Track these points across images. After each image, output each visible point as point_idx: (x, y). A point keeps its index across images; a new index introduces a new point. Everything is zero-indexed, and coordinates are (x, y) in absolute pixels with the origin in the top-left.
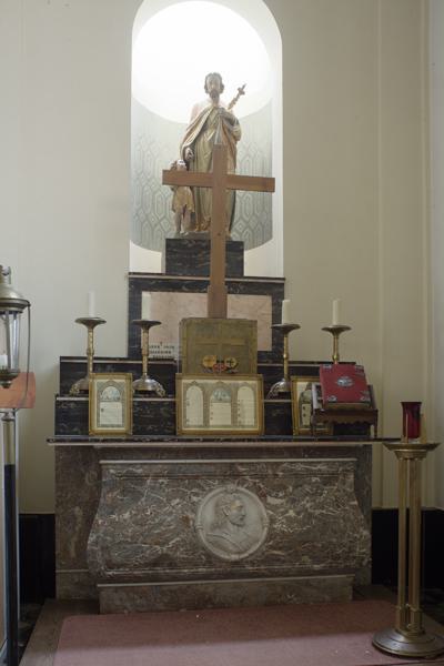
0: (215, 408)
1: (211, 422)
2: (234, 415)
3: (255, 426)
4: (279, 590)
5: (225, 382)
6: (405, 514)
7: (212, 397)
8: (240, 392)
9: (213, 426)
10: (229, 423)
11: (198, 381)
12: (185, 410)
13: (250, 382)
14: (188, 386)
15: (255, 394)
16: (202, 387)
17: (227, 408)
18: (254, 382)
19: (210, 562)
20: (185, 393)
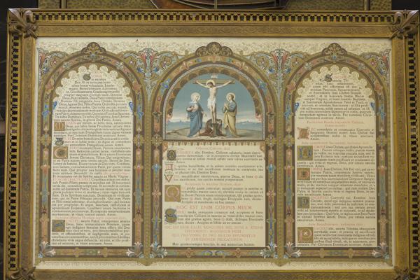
0: (188, 164)
1: (172, 236)
2: (281, 204)
3: (383, 255)
4: (275, 257)
5: (234, 44)
6: (47, 226)
7: (178, 118)
8: (310, 92)
9: (179, 253)
10: (257, 237)
11: (116, 45)
12: (46, 175)
13: (357, 46)
14: (59, 68)
15: (379, 101)
16: (129, 70)
17: (245, 166)
18: (380, 46)
19: (373, 30)
20: (48, 100)
